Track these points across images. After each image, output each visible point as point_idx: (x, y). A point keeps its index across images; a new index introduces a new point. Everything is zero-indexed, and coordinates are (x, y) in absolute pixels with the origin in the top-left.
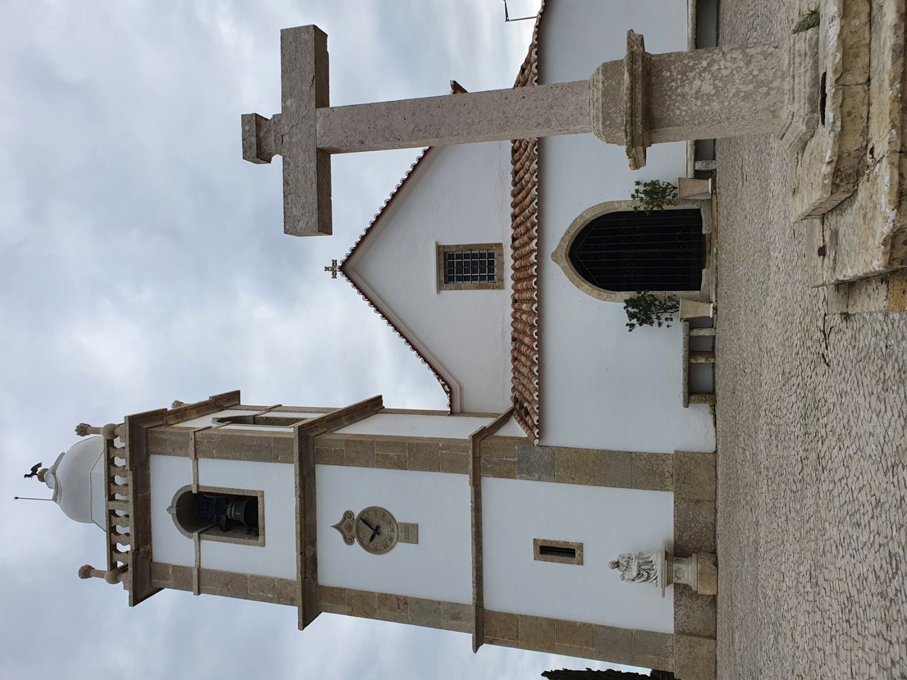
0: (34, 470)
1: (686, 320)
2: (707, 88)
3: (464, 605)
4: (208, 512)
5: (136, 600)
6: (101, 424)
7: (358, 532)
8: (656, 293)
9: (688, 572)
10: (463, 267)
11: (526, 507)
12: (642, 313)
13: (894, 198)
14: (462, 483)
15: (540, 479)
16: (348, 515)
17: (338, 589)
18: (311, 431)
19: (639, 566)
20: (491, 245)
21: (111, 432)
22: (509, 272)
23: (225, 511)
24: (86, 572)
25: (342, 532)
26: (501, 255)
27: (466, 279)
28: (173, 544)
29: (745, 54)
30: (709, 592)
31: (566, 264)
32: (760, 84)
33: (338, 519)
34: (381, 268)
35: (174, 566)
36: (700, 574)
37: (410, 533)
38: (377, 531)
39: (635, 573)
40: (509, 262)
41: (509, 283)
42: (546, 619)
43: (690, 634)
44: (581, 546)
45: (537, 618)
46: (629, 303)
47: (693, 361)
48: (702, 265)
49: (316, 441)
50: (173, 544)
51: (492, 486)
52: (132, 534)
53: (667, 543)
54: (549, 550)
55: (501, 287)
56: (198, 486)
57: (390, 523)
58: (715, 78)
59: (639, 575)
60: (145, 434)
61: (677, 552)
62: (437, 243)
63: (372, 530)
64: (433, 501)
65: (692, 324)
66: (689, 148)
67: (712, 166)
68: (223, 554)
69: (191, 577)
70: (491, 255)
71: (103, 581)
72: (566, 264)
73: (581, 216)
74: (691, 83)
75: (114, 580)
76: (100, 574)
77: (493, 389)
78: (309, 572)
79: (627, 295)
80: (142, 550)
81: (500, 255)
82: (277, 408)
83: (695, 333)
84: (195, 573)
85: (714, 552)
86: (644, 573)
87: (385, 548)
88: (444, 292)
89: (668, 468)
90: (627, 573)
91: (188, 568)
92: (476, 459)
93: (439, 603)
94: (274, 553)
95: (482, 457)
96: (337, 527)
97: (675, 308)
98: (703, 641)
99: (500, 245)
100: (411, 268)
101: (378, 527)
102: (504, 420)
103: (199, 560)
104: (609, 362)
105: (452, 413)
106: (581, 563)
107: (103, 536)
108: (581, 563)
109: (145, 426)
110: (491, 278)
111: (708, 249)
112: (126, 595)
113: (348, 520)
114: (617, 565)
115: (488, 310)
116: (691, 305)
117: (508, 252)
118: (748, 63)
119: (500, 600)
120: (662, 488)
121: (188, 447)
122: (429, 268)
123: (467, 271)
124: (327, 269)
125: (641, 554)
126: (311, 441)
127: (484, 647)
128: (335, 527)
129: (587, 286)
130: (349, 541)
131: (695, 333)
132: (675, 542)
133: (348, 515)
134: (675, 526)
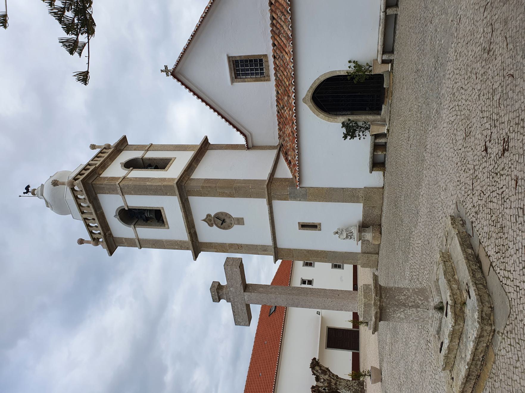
0: (27, 188)
1: (373, 135)
2: (402, 316)
3: (268, 246)
7: (214, 222)
9: (368, 236)
10: (245, 68)
12: (351, 131)
13: (464, 336)
14: (263, 202)
15: (300, 200)
16: (209, 215)
17: (209, 243)
18: (182, 181)
19: (347, 234)
20: (261, 56)
22: (272, 72)
23: (144, 214)
24: (81, 242)
25: (207, 222)
26: (267, 61)
28: (121, 230)
29: (417, 310)
30: (377, 243)
31: (311, 104)
32: (421, 318)
33: (205, 217)
34: (196, 72)
35: (125, 239)
36: (374, 237)
37: (240, 221)
38: (224, 221)
39: (345, 237)
40: (272, 66)
41: (273, 78)
42: (305, 250)
43: (368, 253)
44: (320, 224)
45: (301, 250)
46: (344, 125)
47: (375, 153)
48: (383, 103)
50: (121, 230)
51: (277, 204)
52: (86, 198)
53: (360, 222)
55: (269, 80)
56: (128, 206)
57: (230, 218)
58: (405, 314)
59: (347, 237)
61: (363, 226)
62: (227, 55)
63: (221, 221)
66: (380, 35)
67: (392, 58)
69: (135, 242)
70: (261, 60)
73: (318, 79)
74: (396, 314)
76: (88, 242)
78: (194, 238)
79: (342, 119)
80: (107, 234)
81: (266, 61)
84: (137, 241)
85: (380, 225)
86: (349, 236)
87: (229, 227)
88: (236, 84)
89: (361, 194)
90: (341, 236)
91: (133, 239)
92: (269, 194)
93: (257, 246)
96: (204, 220)
98: (373, 255)
99: (266, 56)
100: (214, 71)
101: (224, 220)
104: (333, 151)
105: (248, 148)
107: (82, 223)
109: (90, 182)
110: (262, 74)
111: (386, 95)
112: (105, 252)
113: (209, 218)
114: (337, 233)
117: (271, 60)
118: (417, 313)
120: (358, 202)
121: (117, 190)
122: (225, 70)
123: (247, 66)
124: (162, 71)
125: (348, 228)
126: (183, 187)
128: (203, 220)
129: (322, 79)
132: (363, 222)
133: (209, 215)
134: (363, 216)
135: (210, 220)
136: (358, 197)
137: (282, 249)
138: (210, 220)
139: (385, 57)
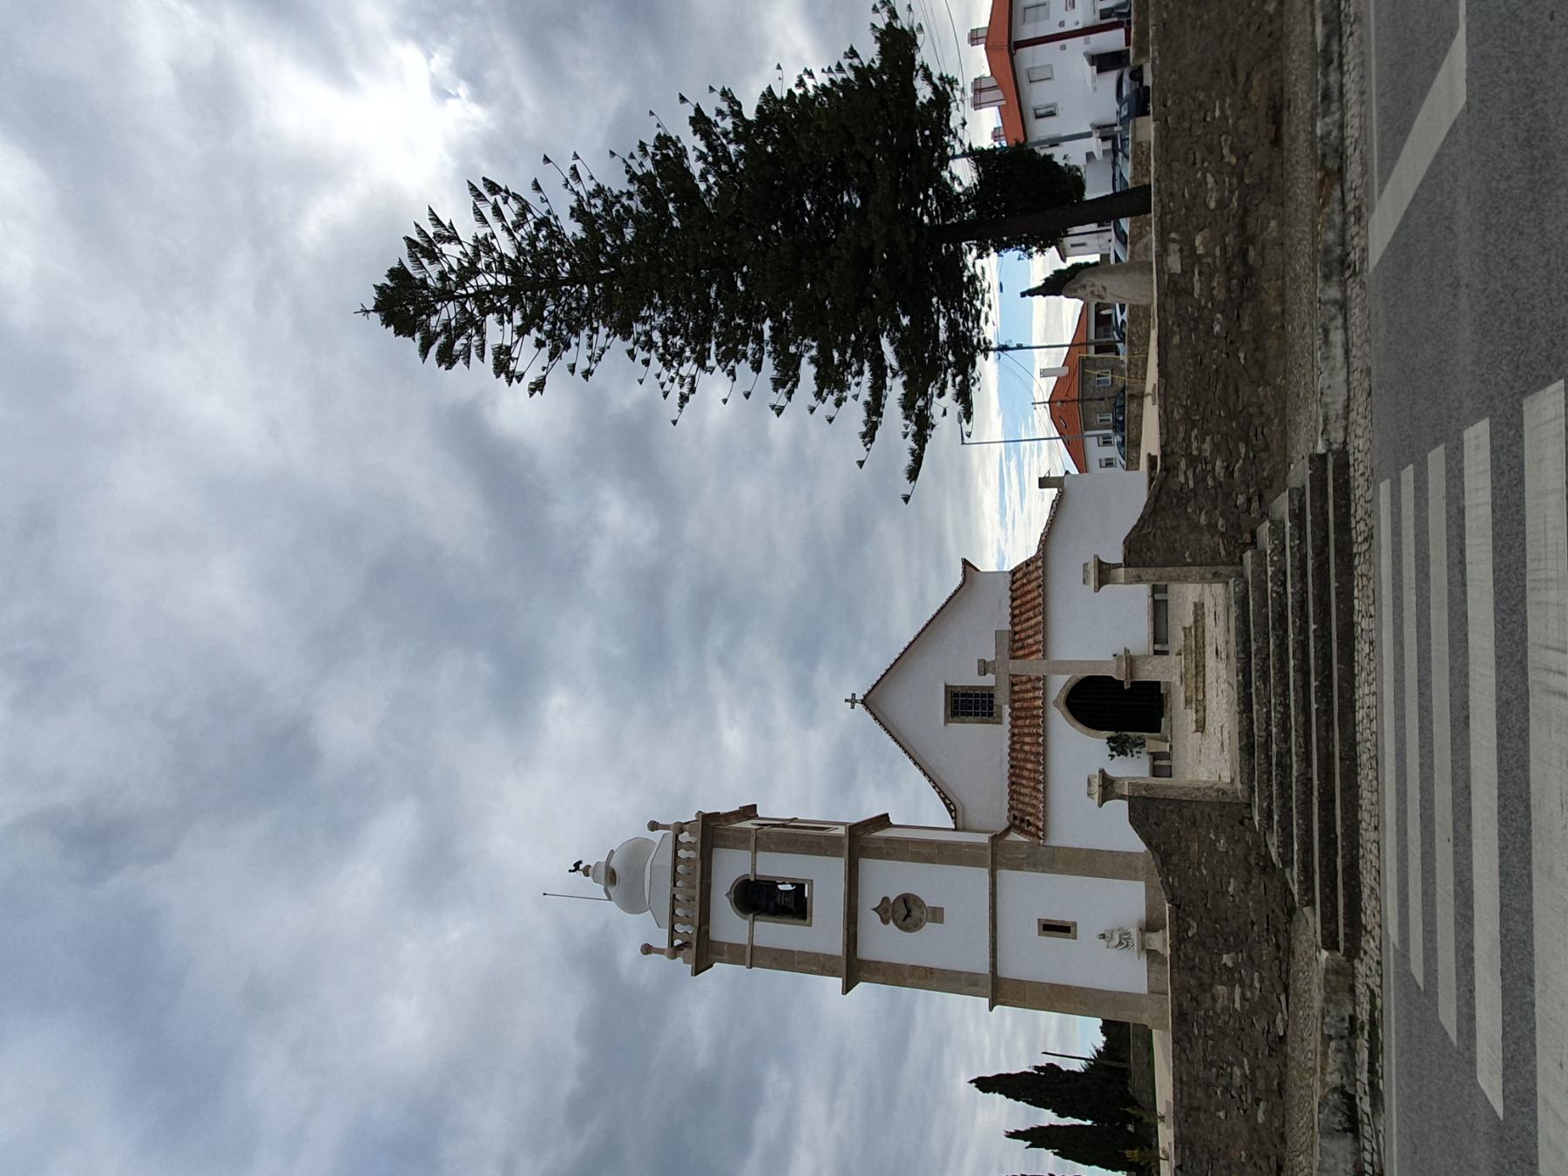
0: (577, 865)
4: (758, 898)
5: (697, 971)
6: (671, 822)
8: (1130, 734)
10: (967, 704)
11: (1032, 894)
16: (885, 900)
21: (680, 828)
22: (1007, 710)
24: (647, 949)
27: (969, 714)
34: (899, 703)
37: (937, 915)
41: (1007, 719)
44: (1075, 924)
46: (1110, 740)
49: (864, 840)
50: (730, 925)
51: (1005, 875)
54: (1049, 928)
55: (1000, 723)
60: (713, 830)
63: (906, 912)
64: (957, 890)
65: (1155, 756)
68: (774, 933)
70: (992, 696)
71: (664, 958)
72: (1064, 709)
75: (673, 956)
76: (660, 951)
77: (990, 805)
82: (794, 820)
83: (1158, 763)
86: (1124, 942)
92: (994, 855)
94: (822, 932)
95: (997, 856)
97: (1143, 744)
102: (1007, 831)
103: (751, 939)
106: (1075, 938)
108: (1075, 938)
110: (991, 715)
114: (1103, 936)
115: (988, 742)
116: (1153, 743)
119: (1012, 968)
127: (997, 1008)
129: (1080, 726)
130: (885, 922)
131: (1158, 763)
133: (885, 900)
135: (886, 911)
136: (1135, 869)
137: (1006, 980)
138: (886, 911)
139: (1158, 647)
